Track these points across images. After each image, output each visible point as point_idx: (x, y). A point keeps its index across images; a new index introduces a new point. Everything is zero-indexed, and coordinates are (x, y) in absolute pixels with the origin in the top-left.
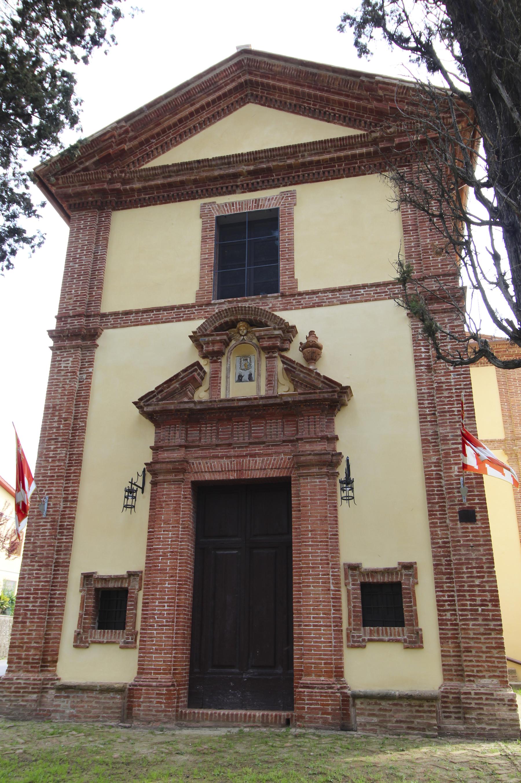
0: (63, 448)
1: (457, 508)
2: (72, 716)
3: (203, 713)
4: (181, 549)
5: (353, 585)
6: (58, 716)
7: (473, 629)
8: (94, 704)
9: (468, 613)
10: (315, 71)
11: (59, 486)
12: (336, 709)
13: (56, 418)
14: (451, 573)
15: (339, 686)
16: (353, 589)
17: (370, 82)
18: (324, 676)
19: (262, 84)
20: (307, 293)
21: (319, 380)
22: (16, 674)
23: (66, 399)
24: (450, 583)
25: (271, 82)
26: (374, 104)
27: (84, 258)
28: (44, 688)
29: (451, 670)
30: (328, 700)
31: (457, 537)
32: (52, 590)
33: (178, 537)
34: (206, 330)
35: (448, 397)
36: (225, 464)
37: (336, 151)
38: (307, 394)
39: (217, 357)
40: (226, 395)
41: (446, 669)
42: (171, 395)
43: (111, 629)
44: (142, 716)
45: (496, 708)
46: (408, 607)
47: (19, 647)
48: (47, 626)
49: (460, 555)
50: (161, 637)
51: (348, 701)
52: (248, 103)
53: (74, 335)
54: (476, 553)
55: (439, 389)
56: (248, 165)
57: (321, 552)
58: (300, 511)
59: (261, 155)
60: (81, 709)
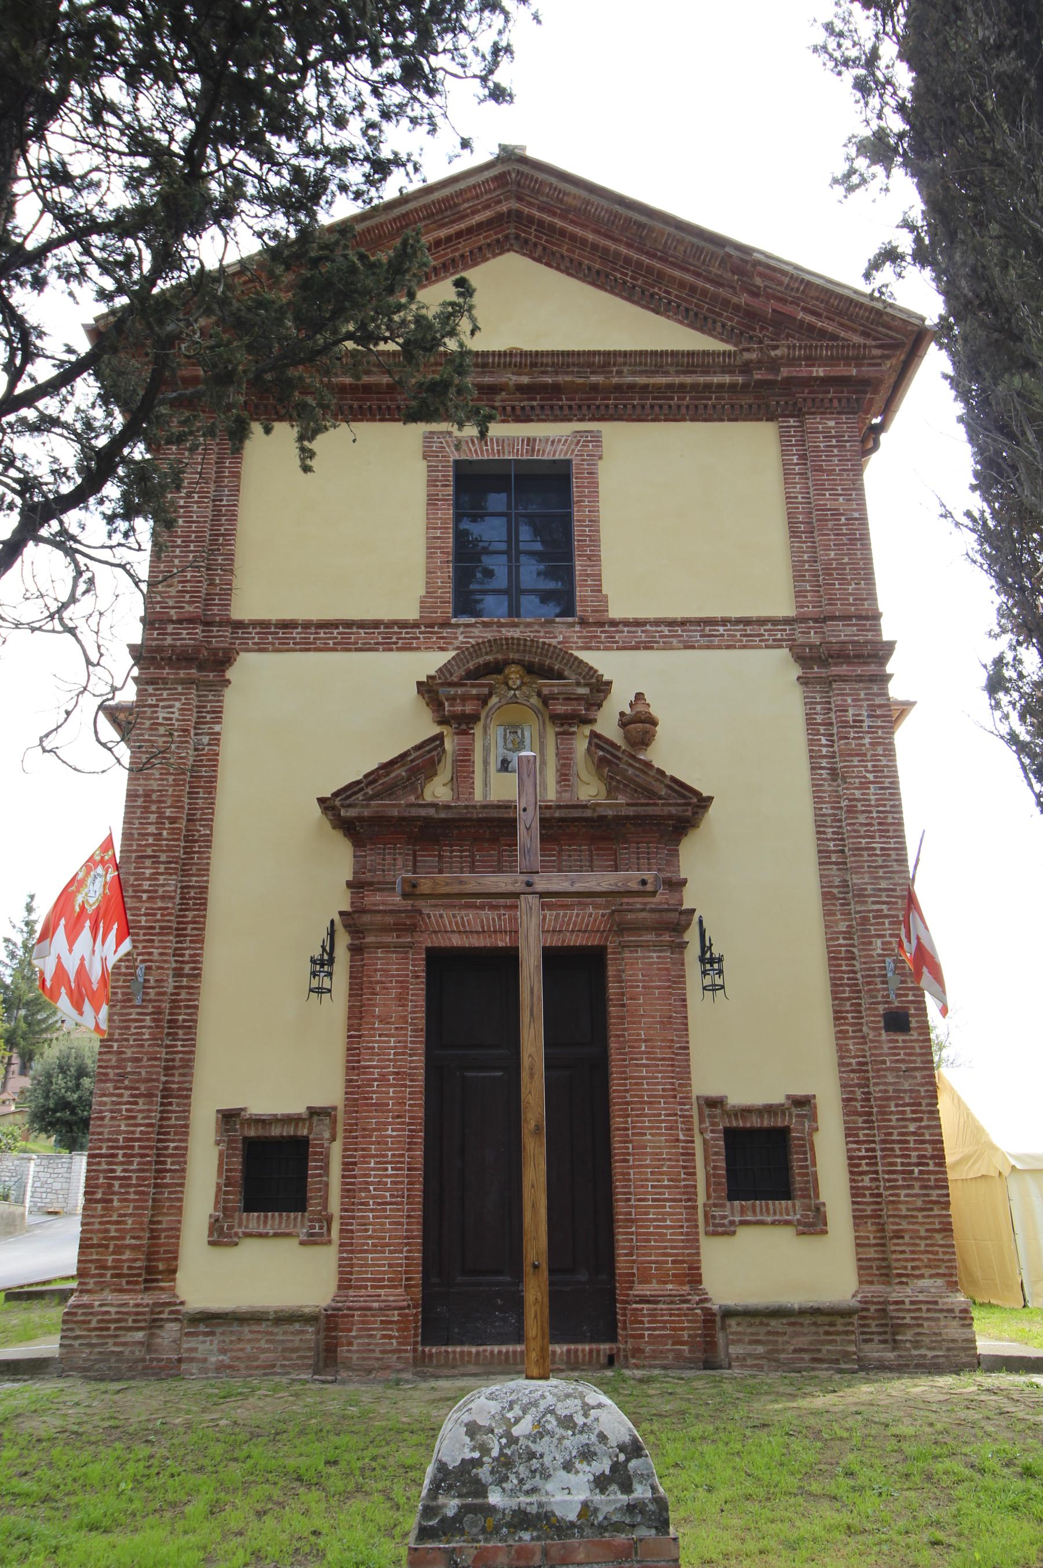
0: (171, 874)
1: (881, 1008)
2: (220, 1368)
3: (462, 1353)
4: (411, 1068)
5: (712, 1131)
6: (194, 1367)
7: (907, 1202)
8: (263, 1344)
9: (899, 1177)
10: (643, 219)
11: (165, 948)
12: (696, 1336)
13: (153, 818)
14: (870, 1114)
15: (697, 1298)
16: (712, 1139)
17: (742, 260)
18: (672, 1282)
19: (541, 223)
20: (626, 623)
21: (662, 782)
22: (96, 1297)
23: (171, 782)
24: (869, 1128)
25: (559, 223)
26: (744, 299)
27: (195, 508)
28: (155, 1320)
29: (871, 1267)
30: (682, 1322)
31: (881, 1055)
32: (159, 1141)
33: (406, 1047)
34: (451, 675)
35: (866, 825)
36: (488, 919)
37: (678, 373)
38: (642, 805)
39: (467, 724)
40: (485, 796)
41: (863, 1266)
42: (389, 791)
43: (280, 1210)
44: (355, 1361)
45: (942, 1323)
46: (801, 1167)
47: (100, 1246)
48: (153, 1208)
49: (886, 1084)
50: (383, 1224)
51: (714, 1321)
52: (508, 250)
53: (184, 658)
54: (910, 1081)
55: (851, 810)
56: (520, 374)
57: (663, 1078)
58: (623, 1005)
59: (545, 360)
60: (240, 1354)
